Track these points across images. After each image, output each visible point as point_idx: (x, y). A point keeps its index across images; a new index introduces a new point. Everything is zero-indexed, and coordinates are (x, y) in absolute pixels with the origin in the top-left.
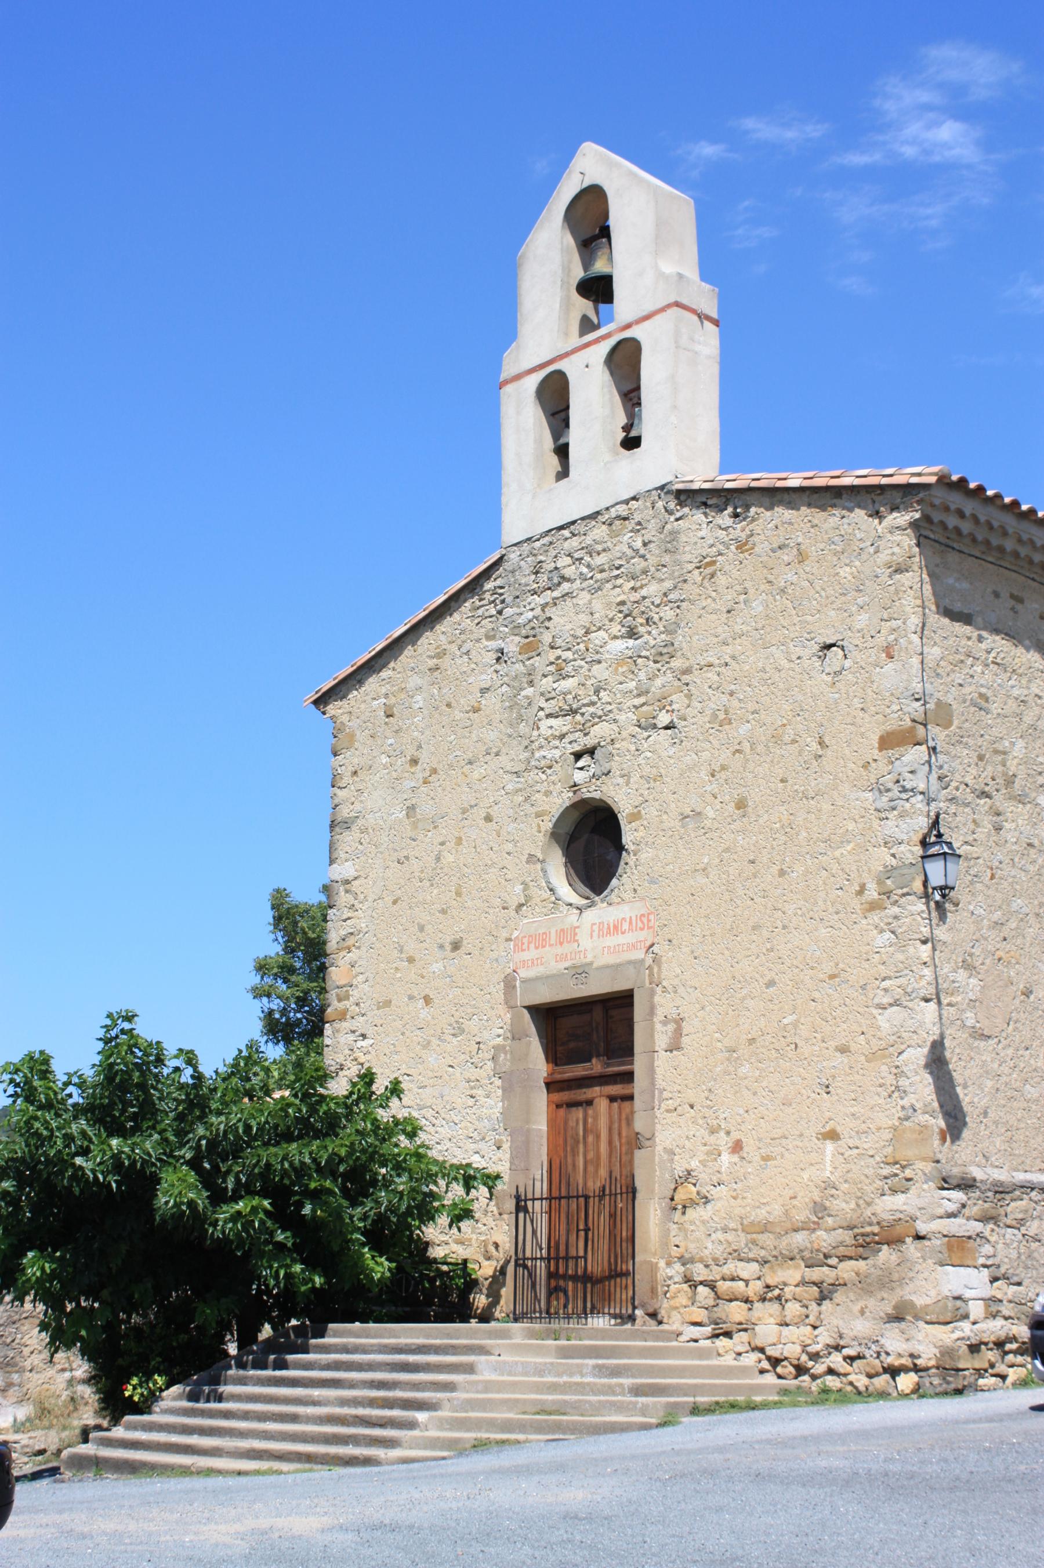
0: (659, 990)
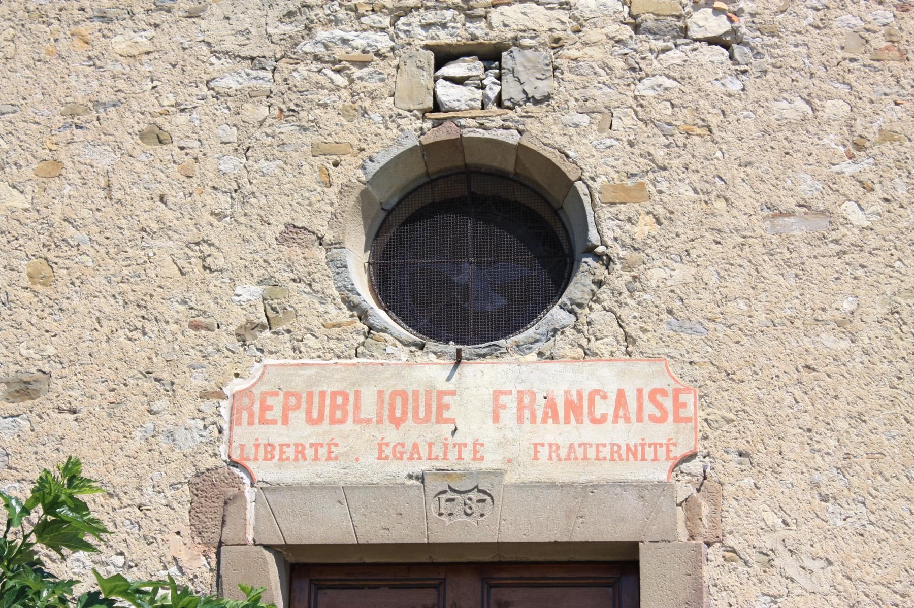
0: (715, 553)
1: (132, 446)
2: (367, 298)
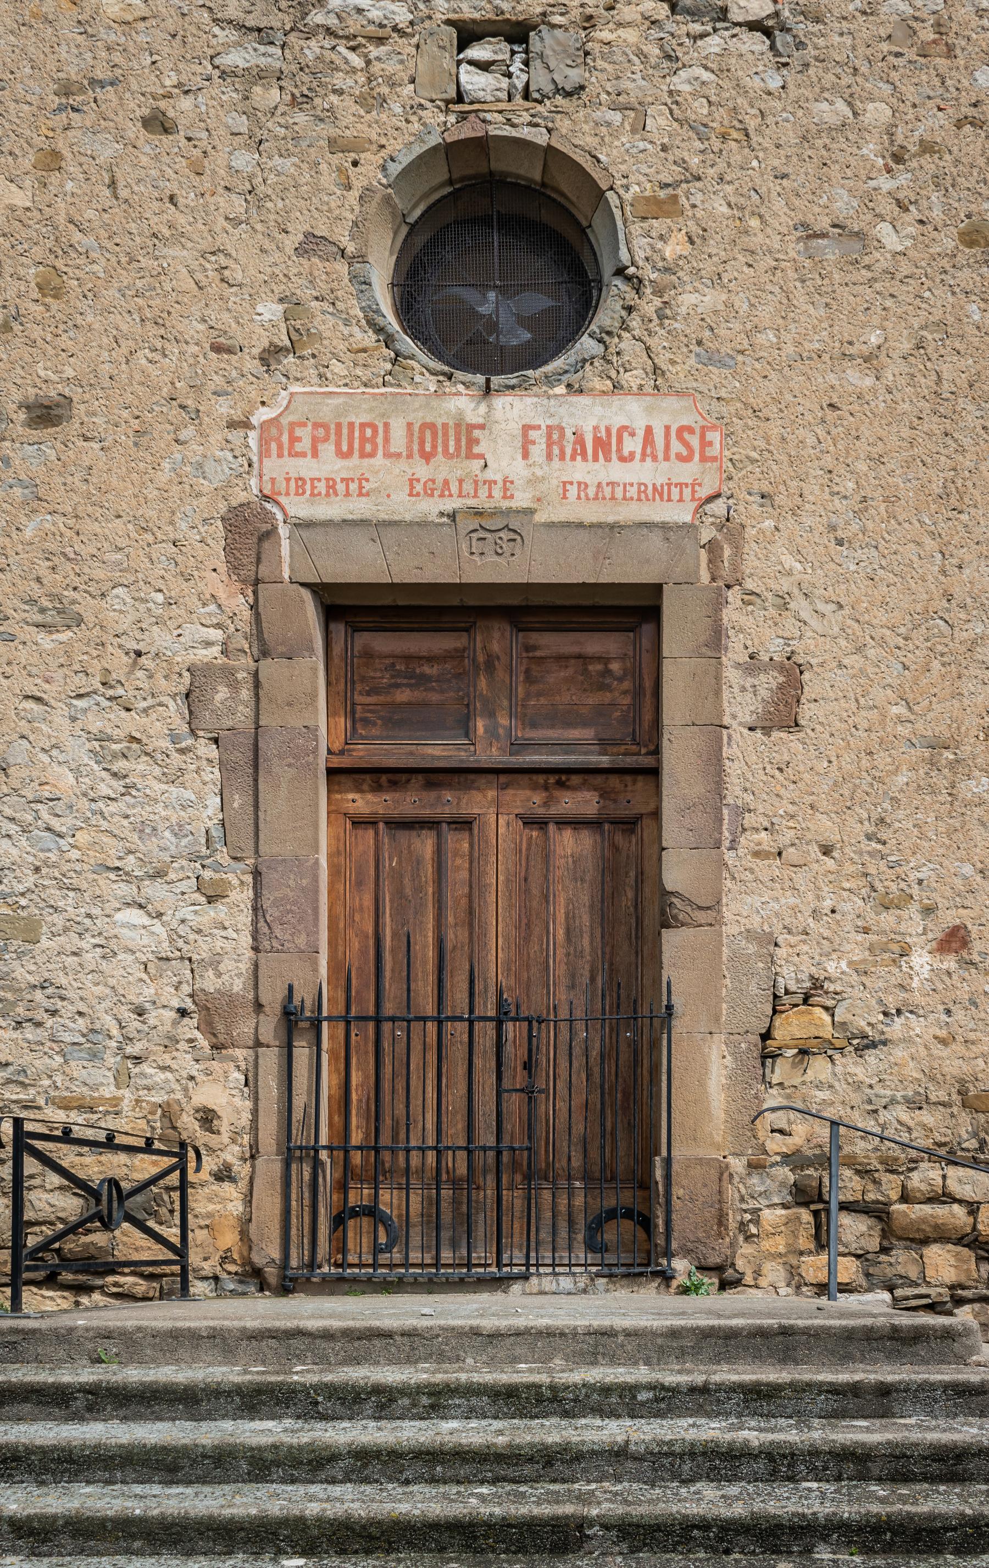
0: (734, 596)
1: (163, 477)
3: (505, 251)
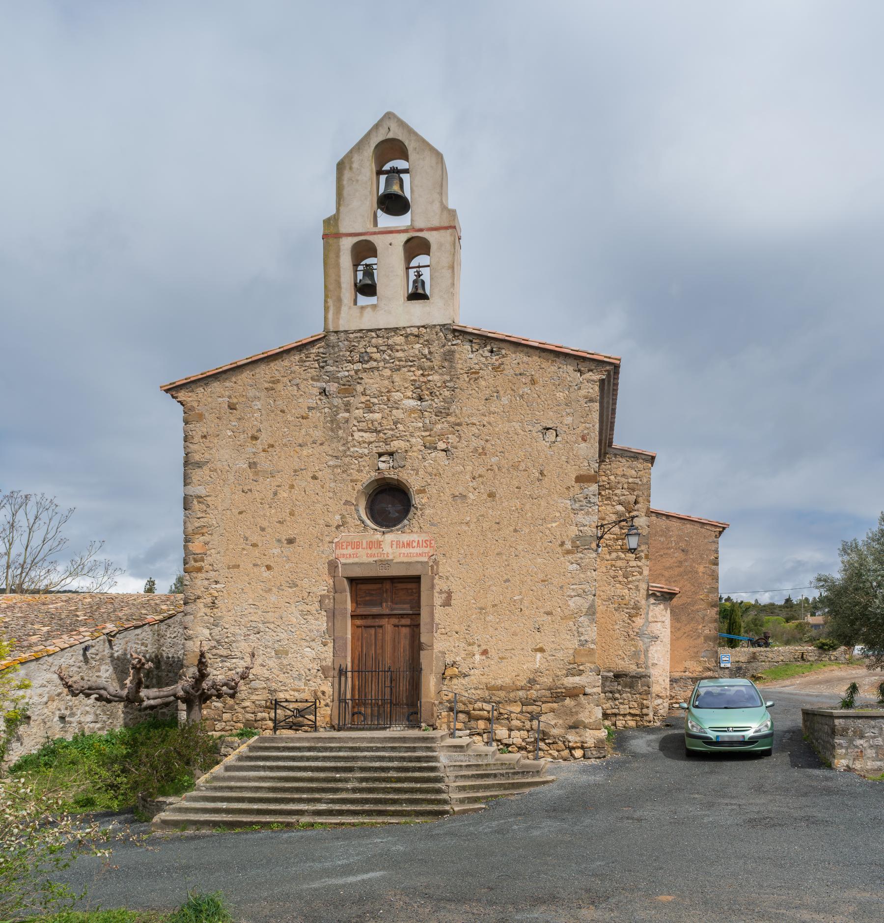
0: (437, 577)
1: (315, 554)
2: (364, 517)
3: (389, 501)
